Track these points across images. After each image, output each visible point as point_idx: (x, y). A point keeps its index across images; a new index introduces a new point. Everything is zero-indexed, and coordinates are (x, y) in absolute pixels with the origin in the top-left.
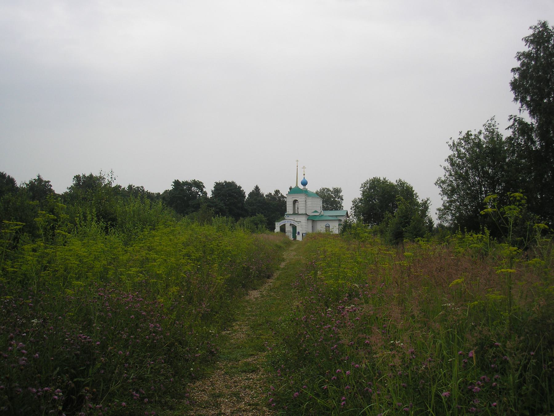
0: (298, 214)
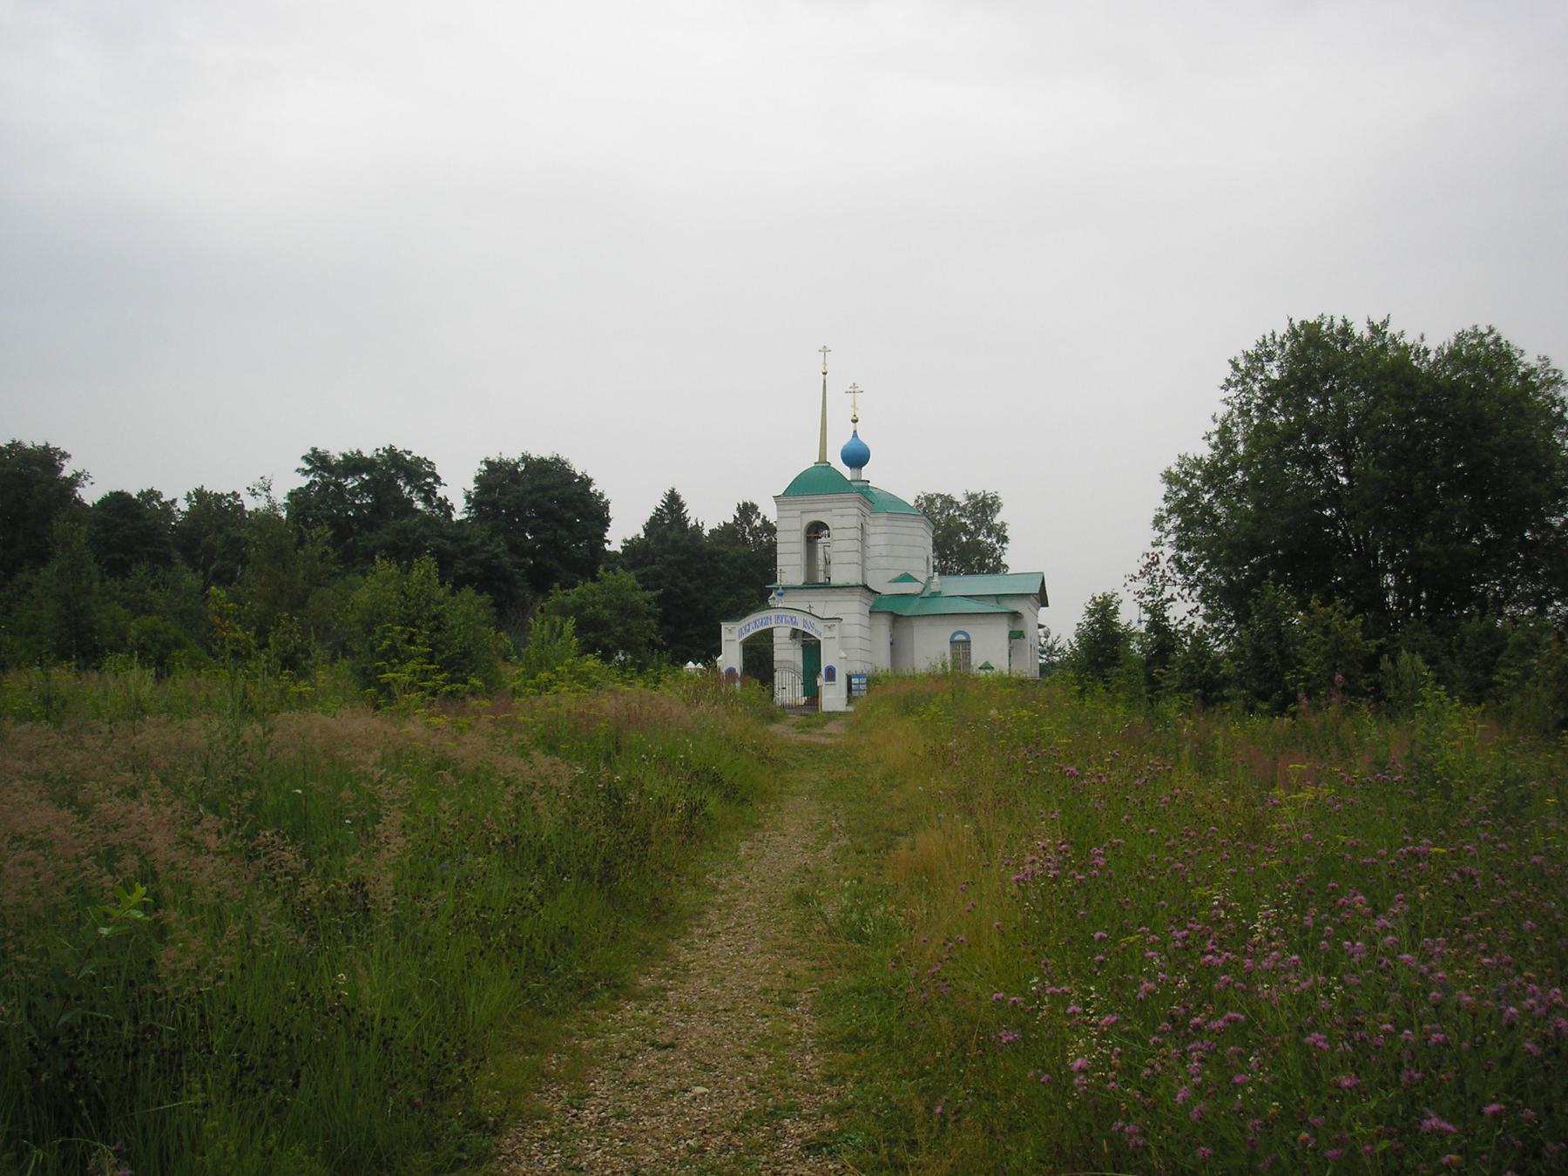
0: (827, 586)
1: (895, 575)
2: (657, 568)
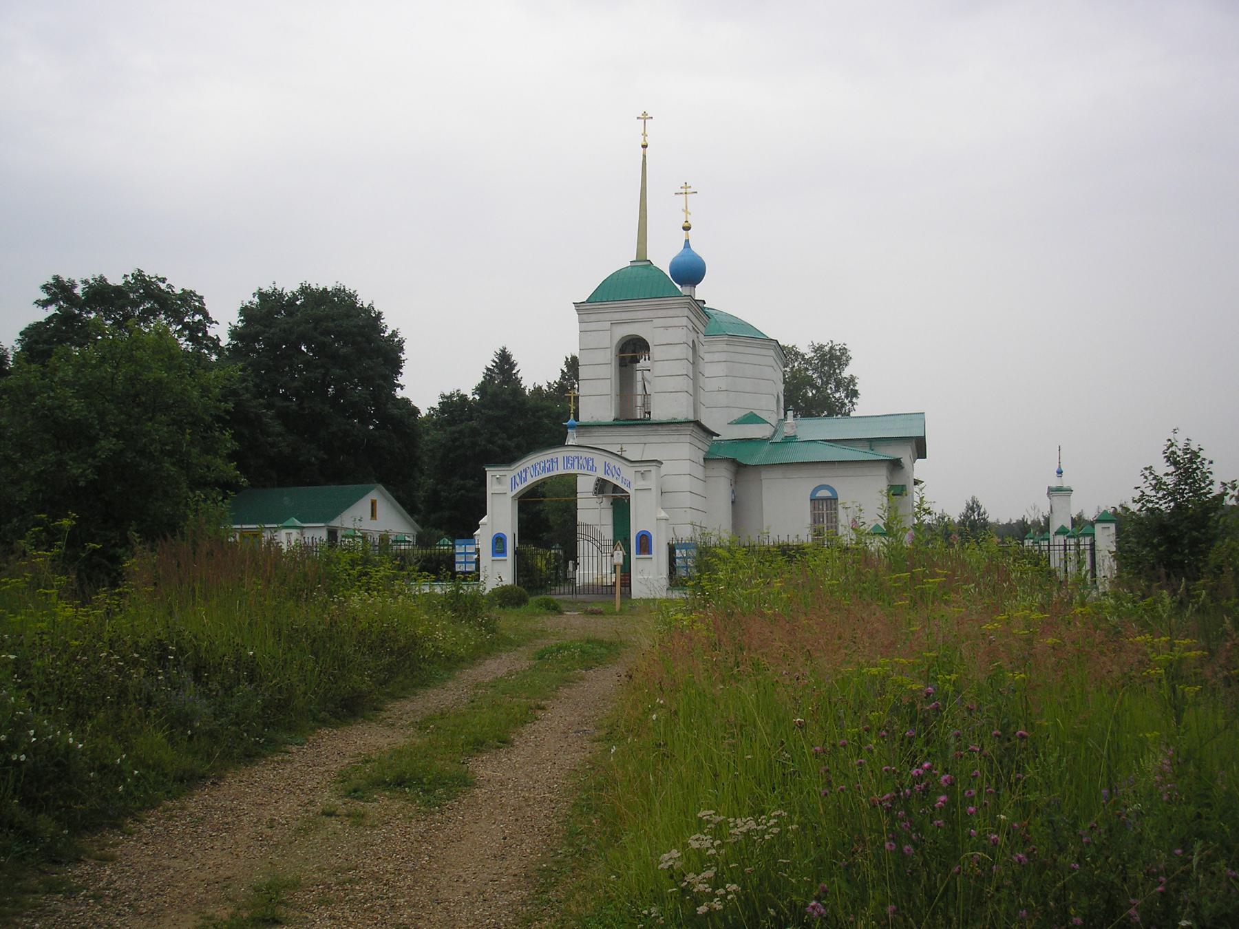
0: (646, 423)
1: (739, 414)
2: (474, 424)
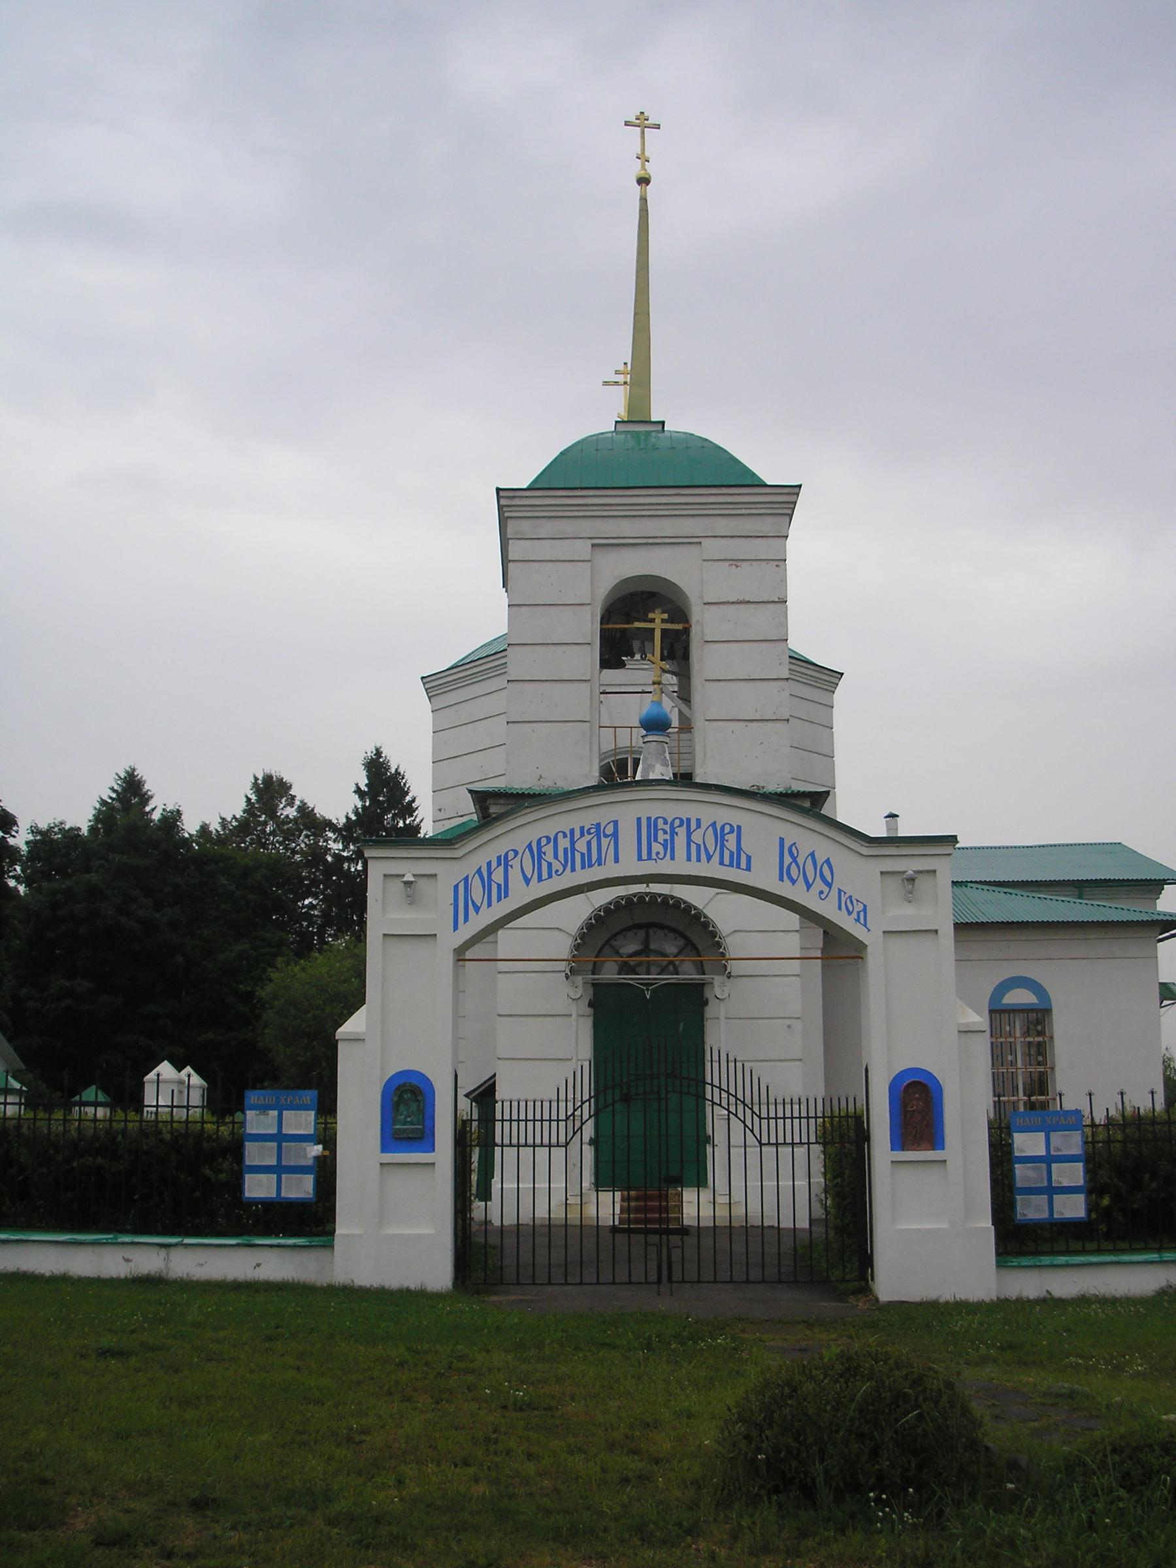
2: (94, 877)
